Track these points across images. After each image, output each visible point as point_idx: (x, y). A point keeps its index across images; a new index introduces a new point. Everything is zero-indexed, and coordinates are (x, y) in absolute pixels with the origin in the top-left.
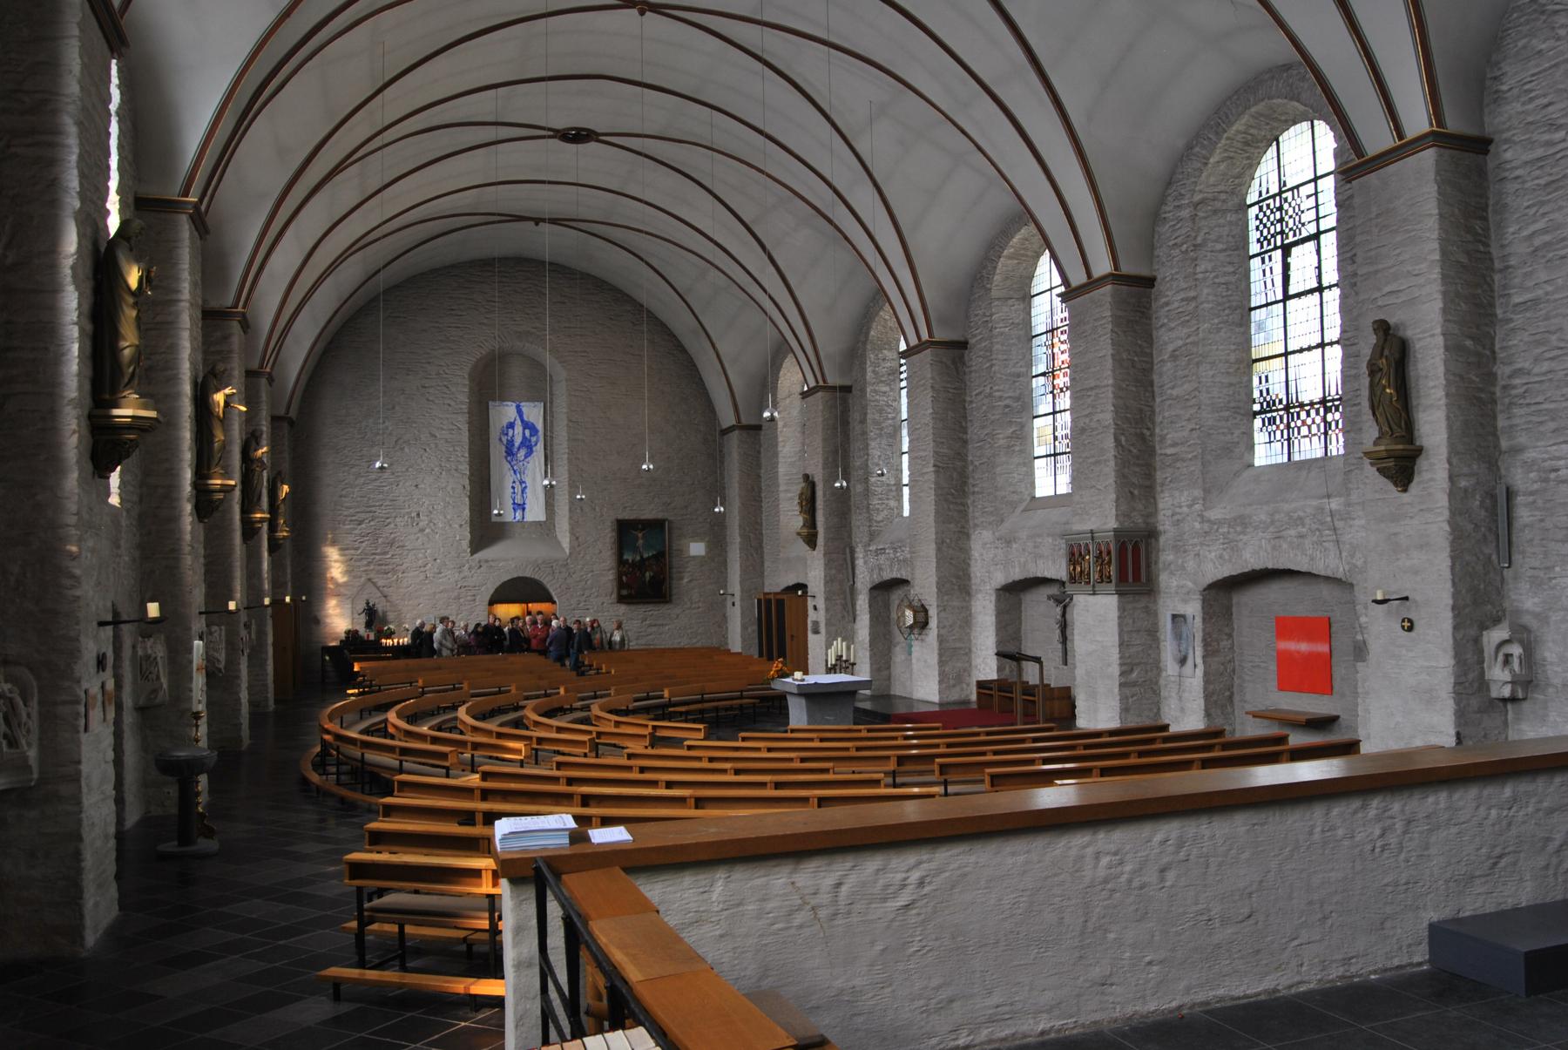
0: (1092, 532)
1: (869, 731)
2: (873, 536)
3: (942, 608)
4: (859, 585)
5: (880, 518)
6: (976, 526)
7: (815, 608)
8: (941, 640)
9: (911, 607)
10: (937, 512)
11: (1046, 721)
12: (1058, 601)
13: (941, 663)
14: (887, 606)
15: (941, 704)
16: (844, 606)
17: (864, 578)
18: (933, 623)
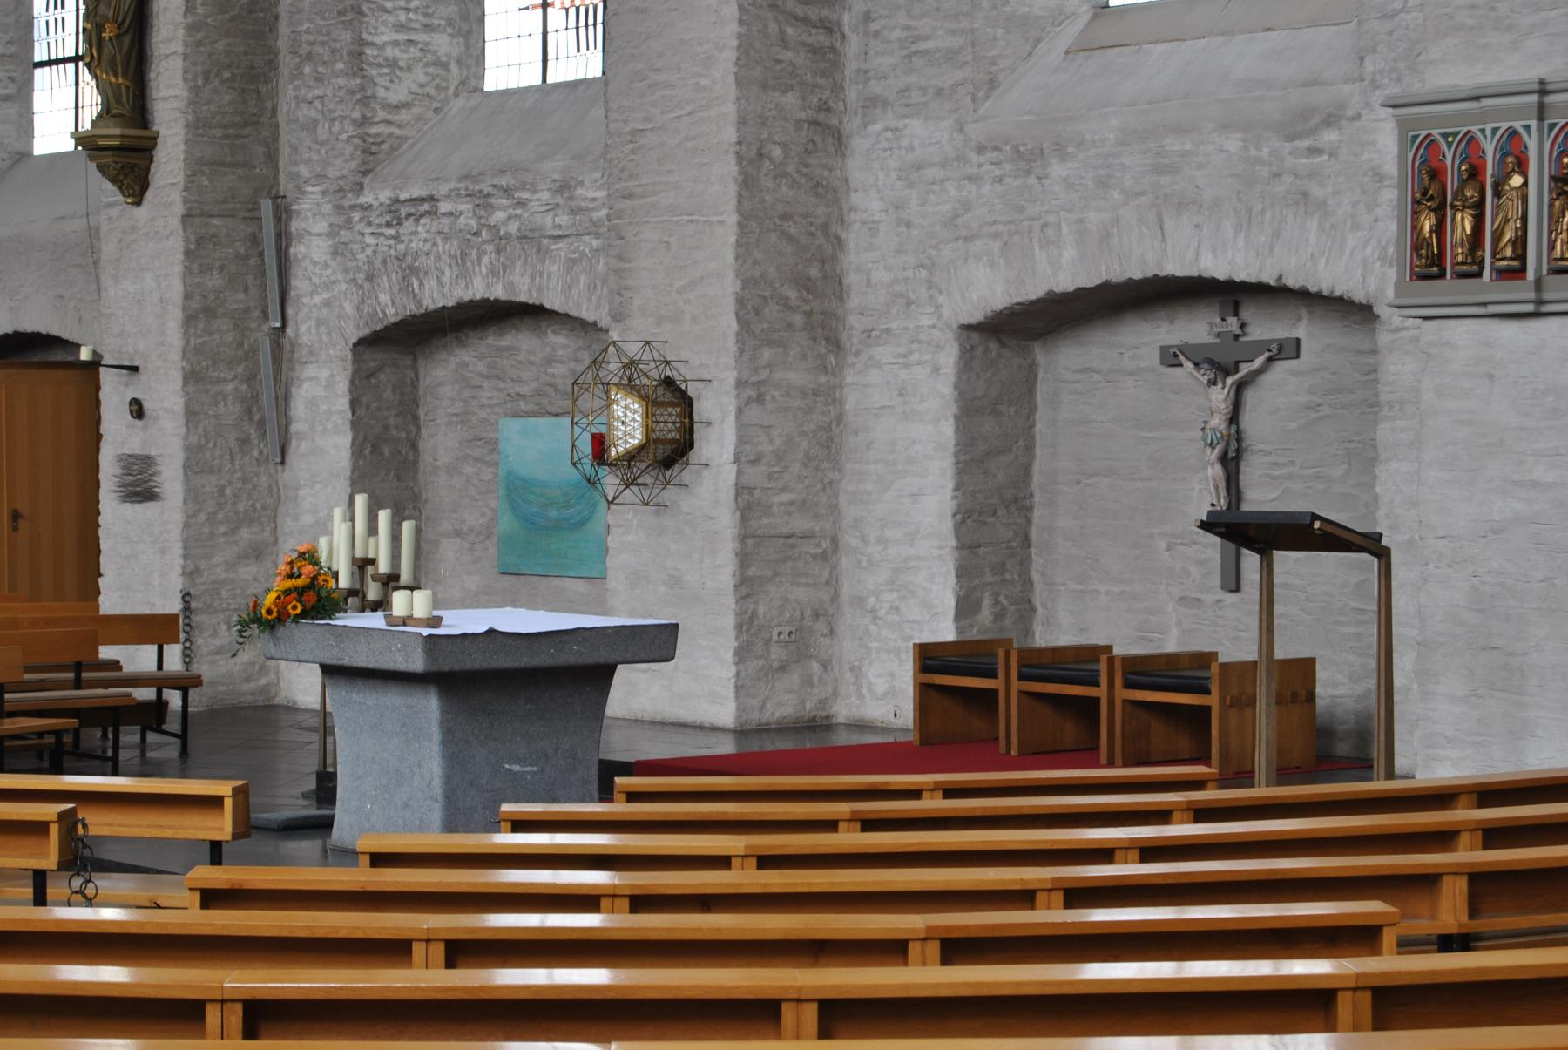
0: (1543, 89)
1: (950, 792)
2: (371, 157)
3: (753, 392)
4: (304, 330)
5: (397, 94)
6: (873, 103)
7: (138, 410)
8: (748, 503)
9: (631, 388)
10: (745, 47)
11: (1284, 774)
12: (1217, 365)
13: (747, 586)
14: (409, 406)
15: (741, 733)
16: (250, 404)
17: (330, 305)
18: (717, 445)
